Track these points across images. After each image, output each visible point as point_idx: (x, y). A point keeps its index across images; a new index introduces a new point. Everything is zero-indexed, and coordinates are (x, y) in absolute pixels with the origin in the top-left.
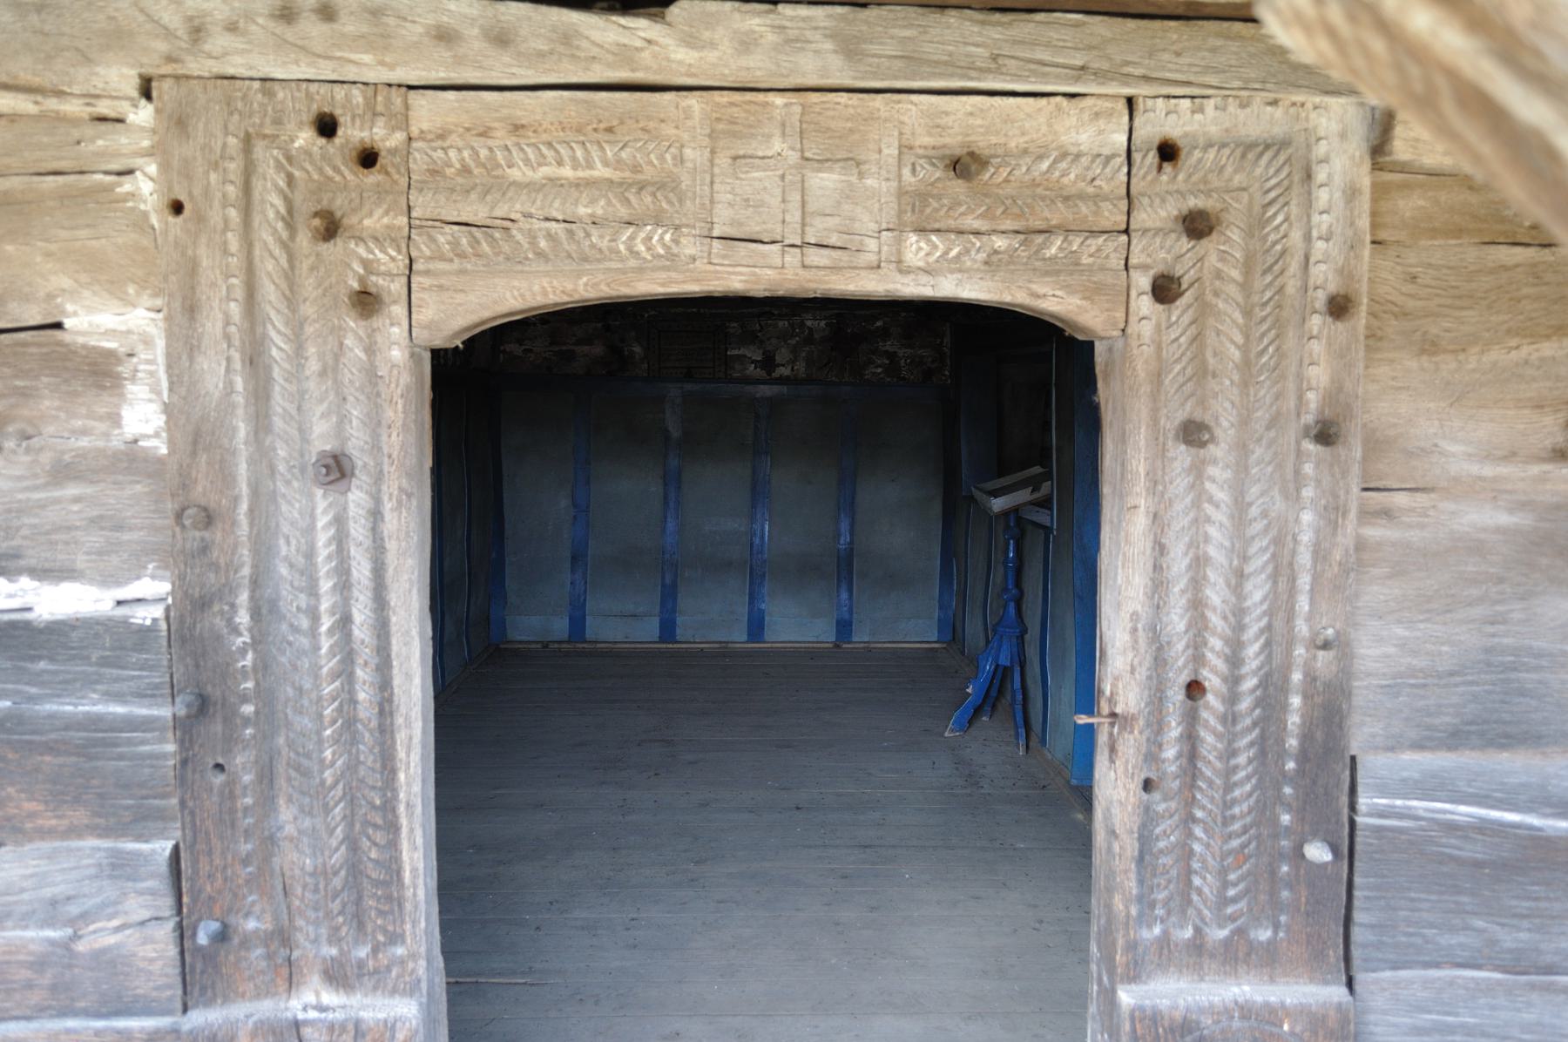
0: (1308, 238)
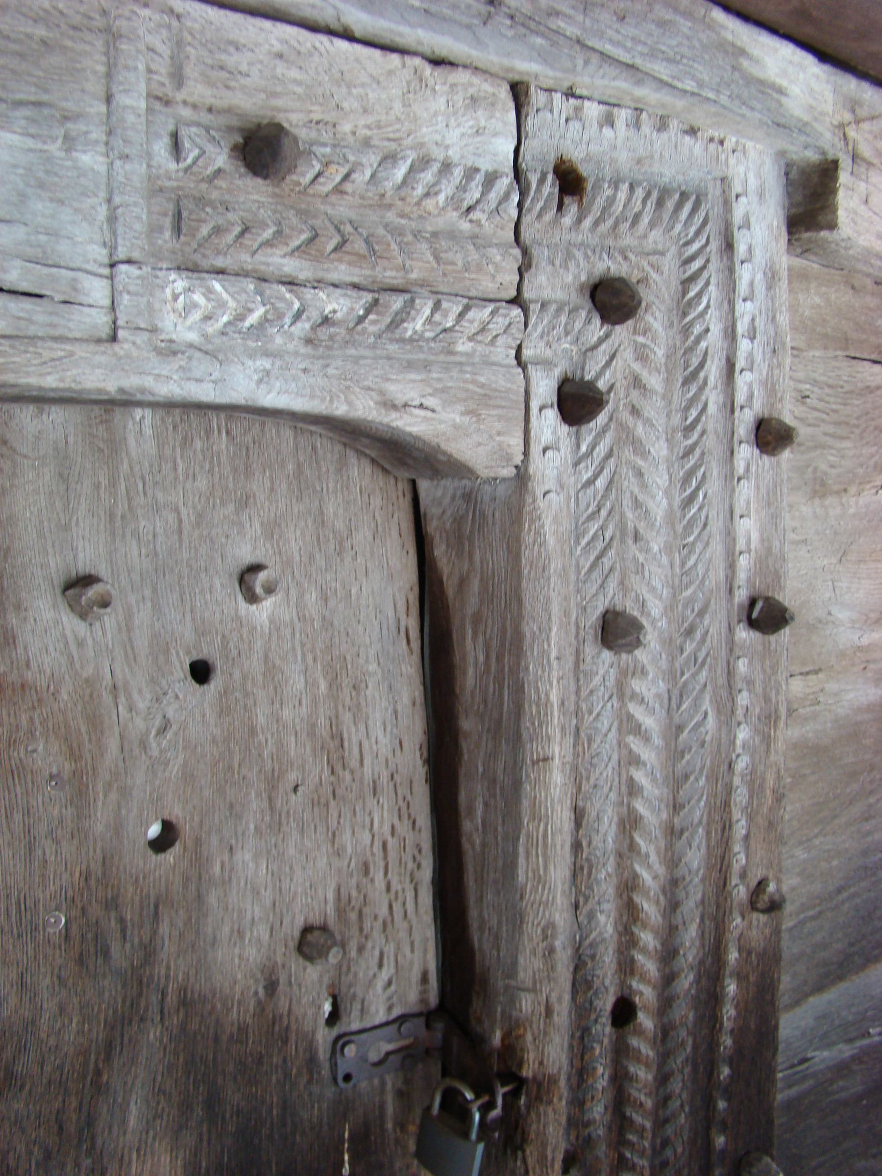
0: (731, 334)
